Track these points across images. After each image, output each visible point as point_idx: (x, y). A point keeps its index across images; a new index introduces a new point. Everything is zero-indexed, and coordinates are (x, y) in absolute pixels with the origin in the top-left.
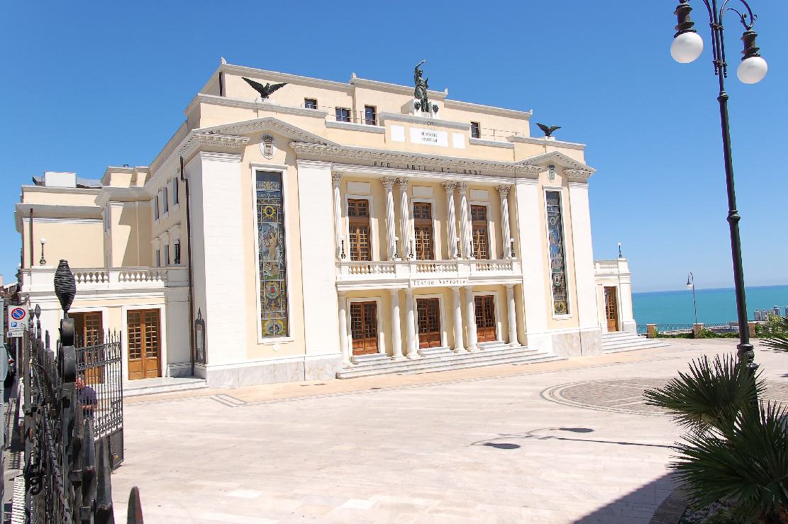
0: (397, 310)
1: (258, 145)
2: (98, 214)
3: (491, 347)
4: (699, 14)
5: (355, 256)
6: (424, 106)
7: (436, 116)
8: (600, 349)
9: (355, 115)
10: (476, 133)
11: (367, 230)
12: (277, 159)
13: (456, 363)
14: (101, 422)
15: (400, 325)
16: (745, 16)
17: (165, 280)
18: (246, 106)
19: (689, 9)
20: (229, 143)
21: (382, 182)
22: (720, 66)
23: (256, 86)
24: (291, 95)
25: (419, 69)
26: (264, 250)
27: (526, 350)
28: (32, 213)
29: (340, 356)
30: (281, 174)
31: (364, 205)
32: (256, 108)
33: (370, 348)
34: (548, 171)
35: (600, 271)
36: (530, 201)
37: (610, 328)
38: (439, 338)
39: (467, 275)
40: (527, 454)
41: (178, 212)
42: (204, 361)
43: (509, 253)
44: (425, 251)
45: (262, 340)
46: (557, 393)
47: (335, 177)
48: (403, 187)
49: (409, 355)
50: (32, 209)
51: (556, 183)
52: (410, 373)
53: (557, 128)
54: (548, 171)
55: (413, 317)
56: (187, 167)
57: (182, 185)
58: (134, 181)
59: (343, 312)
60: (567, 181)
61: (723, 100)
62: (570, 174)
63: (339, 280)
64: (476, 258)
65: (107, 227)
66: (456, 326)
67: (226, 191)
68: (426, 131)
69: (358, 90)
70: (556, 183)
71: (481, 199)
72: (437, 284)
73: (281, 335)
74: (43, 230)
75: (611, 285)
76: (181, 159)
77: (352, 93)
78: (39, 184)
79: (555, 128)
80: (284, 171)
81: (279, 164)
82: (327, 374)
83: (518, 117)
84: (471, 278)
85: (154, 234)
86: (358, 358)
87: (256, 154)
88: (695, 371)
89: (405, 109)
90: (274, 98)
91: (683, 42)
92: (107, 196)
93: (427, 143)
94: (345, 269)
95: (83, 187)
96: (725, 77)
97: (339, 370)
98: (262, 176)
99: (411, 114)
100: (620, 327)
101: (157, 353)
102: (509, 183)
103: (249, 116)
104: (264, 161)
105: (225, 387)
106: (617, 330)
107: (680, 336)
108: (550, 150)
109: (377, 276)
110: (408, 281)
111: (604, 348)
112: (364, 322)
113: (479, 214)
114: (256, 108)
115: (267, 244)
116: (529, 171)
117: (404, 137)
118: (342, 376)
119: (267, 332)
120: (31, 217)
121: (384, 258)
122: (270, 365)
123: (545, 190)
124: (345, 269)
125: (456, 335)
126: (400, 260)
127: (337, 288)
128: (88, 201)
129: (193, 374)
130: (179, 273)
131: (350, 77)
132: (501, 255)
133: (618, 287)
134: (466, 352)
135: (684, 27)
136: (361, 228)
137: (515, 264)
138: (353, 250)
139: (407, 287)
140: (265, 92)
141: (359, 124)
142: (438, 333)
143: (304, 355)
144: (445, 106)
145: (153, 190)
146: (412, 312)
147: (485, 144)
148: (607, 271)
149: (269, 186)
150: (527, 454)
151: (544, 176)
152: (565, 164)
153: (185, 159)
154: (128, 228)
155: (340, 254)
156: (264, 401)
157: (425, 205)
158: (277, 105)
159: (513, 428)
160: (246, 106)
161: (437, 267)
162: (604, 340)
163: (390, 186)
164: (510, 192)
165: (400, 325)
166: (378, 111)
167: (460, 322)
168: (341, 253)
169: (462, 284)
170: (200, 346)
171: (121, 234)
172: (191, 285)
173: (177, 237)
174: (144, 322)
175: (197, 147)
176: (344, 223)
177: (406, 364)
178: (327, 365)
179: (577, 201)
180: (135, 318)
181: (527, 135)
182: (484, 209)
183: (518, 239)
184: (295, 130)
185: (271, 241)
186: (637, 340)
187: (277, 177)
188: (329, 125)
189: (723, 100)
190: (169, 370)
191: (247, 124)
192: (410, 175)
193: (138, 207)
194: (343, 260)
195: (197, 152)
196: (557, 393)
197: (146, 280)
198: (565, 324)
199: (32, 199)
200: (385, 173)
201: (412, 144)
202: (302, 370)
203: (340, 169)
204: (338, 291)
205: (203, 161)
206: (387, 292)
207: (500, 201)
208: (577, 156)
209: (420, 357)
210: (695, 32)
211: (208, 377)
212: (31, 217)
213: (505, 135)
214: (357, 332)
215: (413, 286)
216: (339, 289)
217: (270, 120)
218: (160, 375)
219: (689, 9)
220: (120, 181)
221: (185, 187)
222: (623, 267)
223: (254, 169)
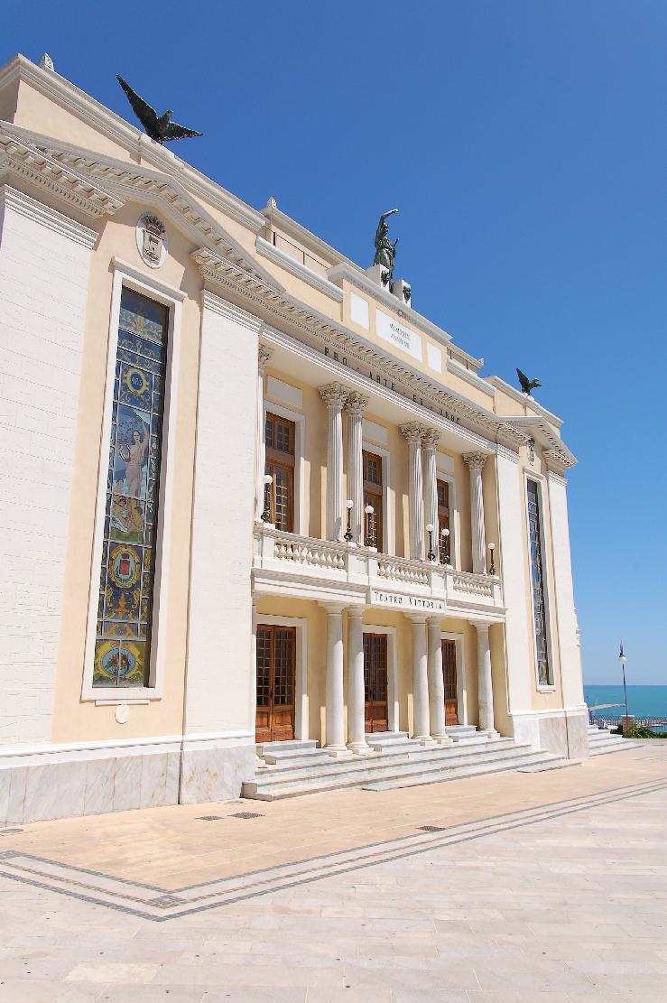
33: (279, 728)
38: (291, 715)
39: (440, 596)
43: (482, 567)
45: (91, 692)
47: (264, 353)
60: (199, 285)
63: (257, 566)
64: (278, 527)
73: (132, 681)
75: (379, 631)
80: (178, 303)
82: (223, 785)
98: (133, 300)
104: (139, 266)
108: (531, 414)
118: (260, 791)
122: (108, 761)
123: (119, 277)
137: (496, 587)
139: (363, 601)
142: (382, 703)
143: (180, 738)
149: (146, 329)
151: (125, 240)
162: (590, 738)
164: (487, 464)
178: (227, 765)
179: (556, 494)
183: (499, 545)
185: (133, 449)
187: (162, 314)
201: (377, 337)
203: (274, 339)
205: (8, 212)
215: (375, 600)
216: (258, 587)
223: (119, 277)
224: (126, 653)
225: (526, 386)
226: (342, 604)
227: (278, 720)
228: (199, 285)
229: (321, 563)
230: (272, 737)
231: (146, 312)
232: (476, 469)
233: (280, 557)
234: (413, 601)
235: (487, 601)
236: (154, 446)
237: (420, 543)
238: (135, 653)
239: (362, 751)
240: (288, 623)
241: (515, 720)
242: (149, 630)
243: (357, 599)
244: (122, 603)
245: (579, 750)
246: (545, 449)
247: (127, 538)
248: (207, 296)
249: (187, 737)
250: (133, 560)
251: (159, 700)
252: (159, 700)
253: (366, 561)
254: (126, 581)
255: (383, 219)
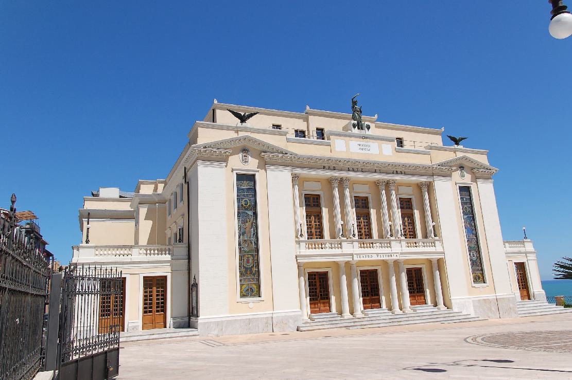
20: (216, 155)
43: (433, 233)
47: (295, 178)
64: (406, 238)
73: (254, 296)
80: (257, 173)
98: (241, 177)
118: (301, 329)
122: (247, 319)
143: (272, 312)
149: (245, 185)
151: (456, 175)
164: (430, 187)
178: (290, 321)
185: (247, 224)
187: (251, 178)
203: (298, 171)
216: (298, 261)
225: (457, 142)
227: (322, 305)
228: (475, 179)
229: (427, 246)
230: (368, 308)
231: (465, 190)
232: (425, 190)
233: (332, 248)
234: (359, 257)
236: (255, 221)
238: (254, 287)
239: (396, 313)
242: (258, 280)
243: (349, 259)
245: (509, 314)
246: (472, 169)
247: (248, 252)
250: (251, 259)
253: (400, 243)
254: (474, 258)
255: (352, 99)
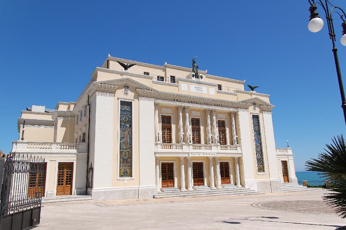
0: (183, 167)
1: (122, 90)
2: (52, 124)
3: (227, 186)
4: (319, 10)
5: (164, 141)
6: (197, 76)
7: (200, 80)
8: (280, 190)
9: (166, 79)
10: (220, 87)
11: (170, 129)
12: (130, 96)
13: (209, 193)
14: (28, 201)
15: (185, 175)
16: (343, 16)
17: (78, 149)
18: (118, 73)
19: (316, 8)
21: (177, 108)
22: (332, 36)
23: (122, 65)
24: (137, 70)
25: (194, 60)
26: (123, 136)
27: (245, 188)
28: (25, 122)
29: (156, 187)
30: (131, 103)
31: (169, 118)
32: (122, 74)
34: (253, 106)
35: (279, 153)
36: (245, 119)
37: (285, 181)
38: (203, 181)
39: (216, 151)
40: (244, 226)
41: (85, 120)
42: (92, 187)
43: (236, 142)
44: (197, 140)
46: (260, 205)
47: (156, 105)
48: (187, 110)
49: (188, 188)
50: (24, 121)
51: (257, 111)
52: (189, 196)
53: (257, 87)
54: (253, 106)
55: (190, 171)
56: (90, 100)
57: (88, 107)
58: (69, 108)
59: (158, 166)
60: (262, 111)
61: (335, 51)
62: (264, 108)
64: (221, 144)
65: (56, 129)
66: (211, 175)
67: (106, 109)
68: (197, 87)
69: (167, 69)
70: (257, 111)
71: (223, 117)
72: (202, 155)
73: (128, 176)
74: (28, 130)
76: (88, 96)
77: (165, 71)
78: (29, 110)
79: (256, 87)
81: (131, 102)
82: (149, 195)
83: (239, 83)
84: (218, 153)
85: (76, 131)
86: (164, 189)
87: (121, 94)
88: (336, 144)
89: (188, 77)
90: (130, 70)
91: (313, 22)
92: (56, 114)
93: (198, 91)
94: (159, 146)
95: (47, 112)
96: (335, 41)
97: (155, 194)
98: (123, 103)
99: (191, 79)
100: (290, 180)
101: (71, 184)
102: (236, 111)
103: (119, 77)
105: (101, 199)
106: (288, 182)
107: (319, 187)
108: (254, 96)
109: (174, 150)
110: (189, 153)
111: (282, 190)
112: (167, 172)
113: (221, 125)
114: (122, 74)
115: (124, 134)
116: (244, 105)
117: (188, 88)
118: (156, 197)
119: (122, 174)
120: (24, 125)
121: (178, 142)
123: (252, 114)
124: (159, 146)
125: (211, 180)
126: (185, 143)
127: (155, 155)
128: (49, 118)
129: (86, 193)
130: (84, 146)
131: (164, 64)
132: (232, 143)
133: (288, 161)
134: (216, 188)
135: (314, 15)
136: (167, 129)
137: (238, 148)
138: (163, 137)
139: (188, 156)
140: (126, 67)
141: (167, 82)
143: (138, 186)
144: (206, 77)
145: (77, 113)
146: (190, 168)
147: (225, 93)
148: (282, 153)
149: (126, 108)
150: (244, 226)
151: (251, 108)
152: (261, 103)
153: (90, 96)
154: (64, 129)
155: (157, 139)
156: (118, 205)
157: (197, 120)
158: (131, 73)
159: (236, 217)
160: (118, 73)
161: (202, 147)
162: (282, 186)
163: (181, 110)
164: (236, 115)
165: (185, 175)
166: (176, 78)
167: (213, 174)
168: (158, 139)
169: (214, 156)
170: (90, 180)
171: (61, 131)
172: (88, 152)
173: (84, 131)
174: (65, 169)
175: (95, 90)
176: (159, 126)
177: (187, 192)
179: (267, 120)
180: (62, 166)
181: (243, 90)
182: (223, 122)
184: (138, 84)
185: (126, 132)
186: (298, 187)
187: (130, 104)
188: (154, 82)
189: (335, 51)
190: (75, 191)
191: (117, 80)
192: (191, 105)
193: (70, 120)
194: (158, 142)
195: (95, 92)
196: (260, 205)
197: (68, 149)
198: (263, 177)
199: (25, 116)
200: (178, 104)
202: (138, 193)
204: (156, 157)
206: (179, 158)
207: (231, 118)
208: (266, 100)
209: (193, 190)
210: (319, 17)
211: (93, 194)
212: (24, 125)
213: (233, 90)
214: (164, 175)
215: (191, 155)
216: (156, 156)
217: (127, 79)
218: (71, 194)
219: (316, 8)
220: (63, 108)
221: (90, 108)
222: (290, 152)
224: (126, 171)
226: (183, 157)
228: (262, 111)
229: (208, 149)
230: (165, 187)
235: (180, 151)
237: (210, 139)
240: (57, 164)
241: (245, 182)
242: (131, 166)
244: (125, 162)
248: (263, 112)
249: (140, 186)
250: (127, 153)
251: (133, 179)
252: (133, 179)
